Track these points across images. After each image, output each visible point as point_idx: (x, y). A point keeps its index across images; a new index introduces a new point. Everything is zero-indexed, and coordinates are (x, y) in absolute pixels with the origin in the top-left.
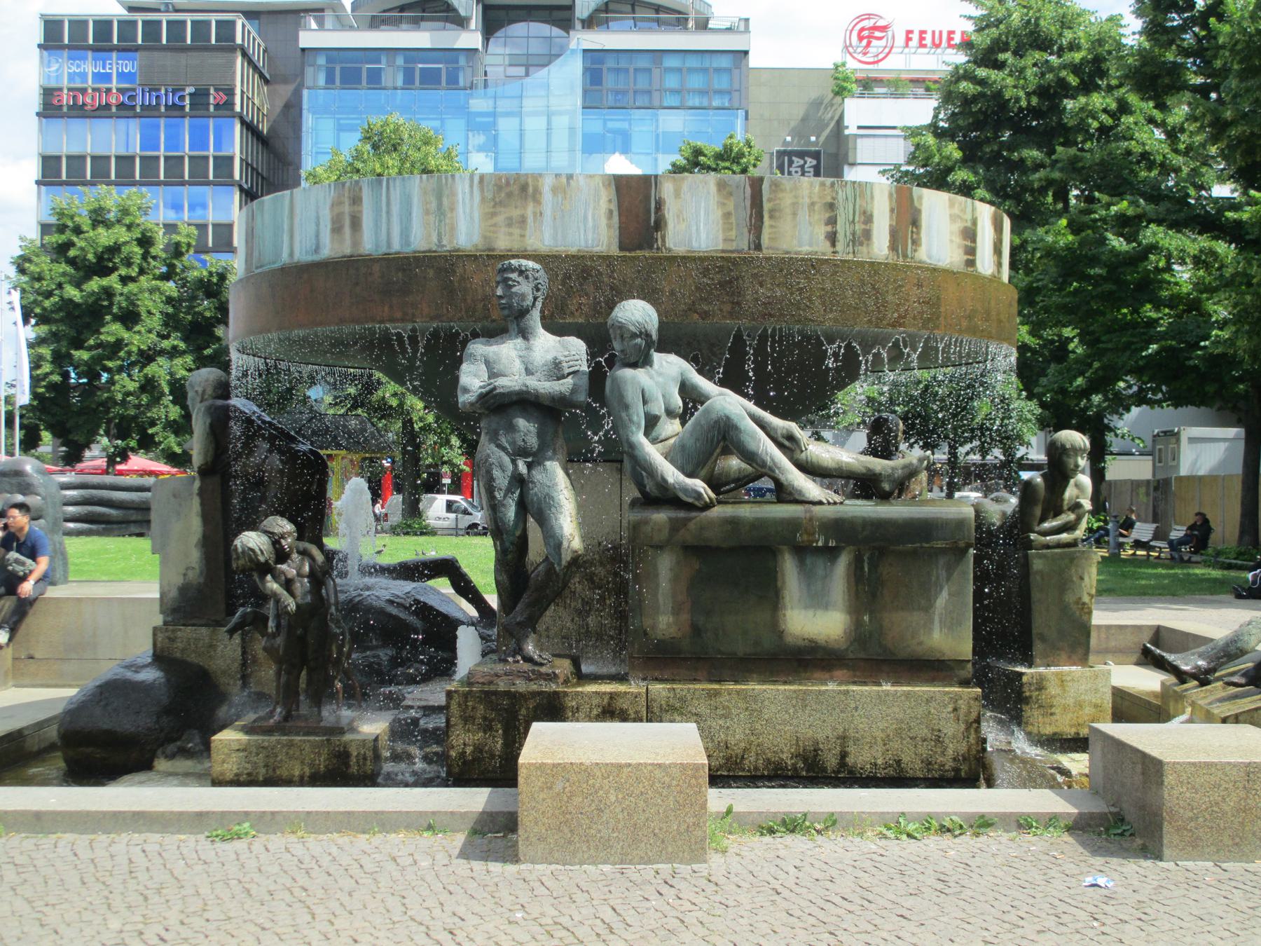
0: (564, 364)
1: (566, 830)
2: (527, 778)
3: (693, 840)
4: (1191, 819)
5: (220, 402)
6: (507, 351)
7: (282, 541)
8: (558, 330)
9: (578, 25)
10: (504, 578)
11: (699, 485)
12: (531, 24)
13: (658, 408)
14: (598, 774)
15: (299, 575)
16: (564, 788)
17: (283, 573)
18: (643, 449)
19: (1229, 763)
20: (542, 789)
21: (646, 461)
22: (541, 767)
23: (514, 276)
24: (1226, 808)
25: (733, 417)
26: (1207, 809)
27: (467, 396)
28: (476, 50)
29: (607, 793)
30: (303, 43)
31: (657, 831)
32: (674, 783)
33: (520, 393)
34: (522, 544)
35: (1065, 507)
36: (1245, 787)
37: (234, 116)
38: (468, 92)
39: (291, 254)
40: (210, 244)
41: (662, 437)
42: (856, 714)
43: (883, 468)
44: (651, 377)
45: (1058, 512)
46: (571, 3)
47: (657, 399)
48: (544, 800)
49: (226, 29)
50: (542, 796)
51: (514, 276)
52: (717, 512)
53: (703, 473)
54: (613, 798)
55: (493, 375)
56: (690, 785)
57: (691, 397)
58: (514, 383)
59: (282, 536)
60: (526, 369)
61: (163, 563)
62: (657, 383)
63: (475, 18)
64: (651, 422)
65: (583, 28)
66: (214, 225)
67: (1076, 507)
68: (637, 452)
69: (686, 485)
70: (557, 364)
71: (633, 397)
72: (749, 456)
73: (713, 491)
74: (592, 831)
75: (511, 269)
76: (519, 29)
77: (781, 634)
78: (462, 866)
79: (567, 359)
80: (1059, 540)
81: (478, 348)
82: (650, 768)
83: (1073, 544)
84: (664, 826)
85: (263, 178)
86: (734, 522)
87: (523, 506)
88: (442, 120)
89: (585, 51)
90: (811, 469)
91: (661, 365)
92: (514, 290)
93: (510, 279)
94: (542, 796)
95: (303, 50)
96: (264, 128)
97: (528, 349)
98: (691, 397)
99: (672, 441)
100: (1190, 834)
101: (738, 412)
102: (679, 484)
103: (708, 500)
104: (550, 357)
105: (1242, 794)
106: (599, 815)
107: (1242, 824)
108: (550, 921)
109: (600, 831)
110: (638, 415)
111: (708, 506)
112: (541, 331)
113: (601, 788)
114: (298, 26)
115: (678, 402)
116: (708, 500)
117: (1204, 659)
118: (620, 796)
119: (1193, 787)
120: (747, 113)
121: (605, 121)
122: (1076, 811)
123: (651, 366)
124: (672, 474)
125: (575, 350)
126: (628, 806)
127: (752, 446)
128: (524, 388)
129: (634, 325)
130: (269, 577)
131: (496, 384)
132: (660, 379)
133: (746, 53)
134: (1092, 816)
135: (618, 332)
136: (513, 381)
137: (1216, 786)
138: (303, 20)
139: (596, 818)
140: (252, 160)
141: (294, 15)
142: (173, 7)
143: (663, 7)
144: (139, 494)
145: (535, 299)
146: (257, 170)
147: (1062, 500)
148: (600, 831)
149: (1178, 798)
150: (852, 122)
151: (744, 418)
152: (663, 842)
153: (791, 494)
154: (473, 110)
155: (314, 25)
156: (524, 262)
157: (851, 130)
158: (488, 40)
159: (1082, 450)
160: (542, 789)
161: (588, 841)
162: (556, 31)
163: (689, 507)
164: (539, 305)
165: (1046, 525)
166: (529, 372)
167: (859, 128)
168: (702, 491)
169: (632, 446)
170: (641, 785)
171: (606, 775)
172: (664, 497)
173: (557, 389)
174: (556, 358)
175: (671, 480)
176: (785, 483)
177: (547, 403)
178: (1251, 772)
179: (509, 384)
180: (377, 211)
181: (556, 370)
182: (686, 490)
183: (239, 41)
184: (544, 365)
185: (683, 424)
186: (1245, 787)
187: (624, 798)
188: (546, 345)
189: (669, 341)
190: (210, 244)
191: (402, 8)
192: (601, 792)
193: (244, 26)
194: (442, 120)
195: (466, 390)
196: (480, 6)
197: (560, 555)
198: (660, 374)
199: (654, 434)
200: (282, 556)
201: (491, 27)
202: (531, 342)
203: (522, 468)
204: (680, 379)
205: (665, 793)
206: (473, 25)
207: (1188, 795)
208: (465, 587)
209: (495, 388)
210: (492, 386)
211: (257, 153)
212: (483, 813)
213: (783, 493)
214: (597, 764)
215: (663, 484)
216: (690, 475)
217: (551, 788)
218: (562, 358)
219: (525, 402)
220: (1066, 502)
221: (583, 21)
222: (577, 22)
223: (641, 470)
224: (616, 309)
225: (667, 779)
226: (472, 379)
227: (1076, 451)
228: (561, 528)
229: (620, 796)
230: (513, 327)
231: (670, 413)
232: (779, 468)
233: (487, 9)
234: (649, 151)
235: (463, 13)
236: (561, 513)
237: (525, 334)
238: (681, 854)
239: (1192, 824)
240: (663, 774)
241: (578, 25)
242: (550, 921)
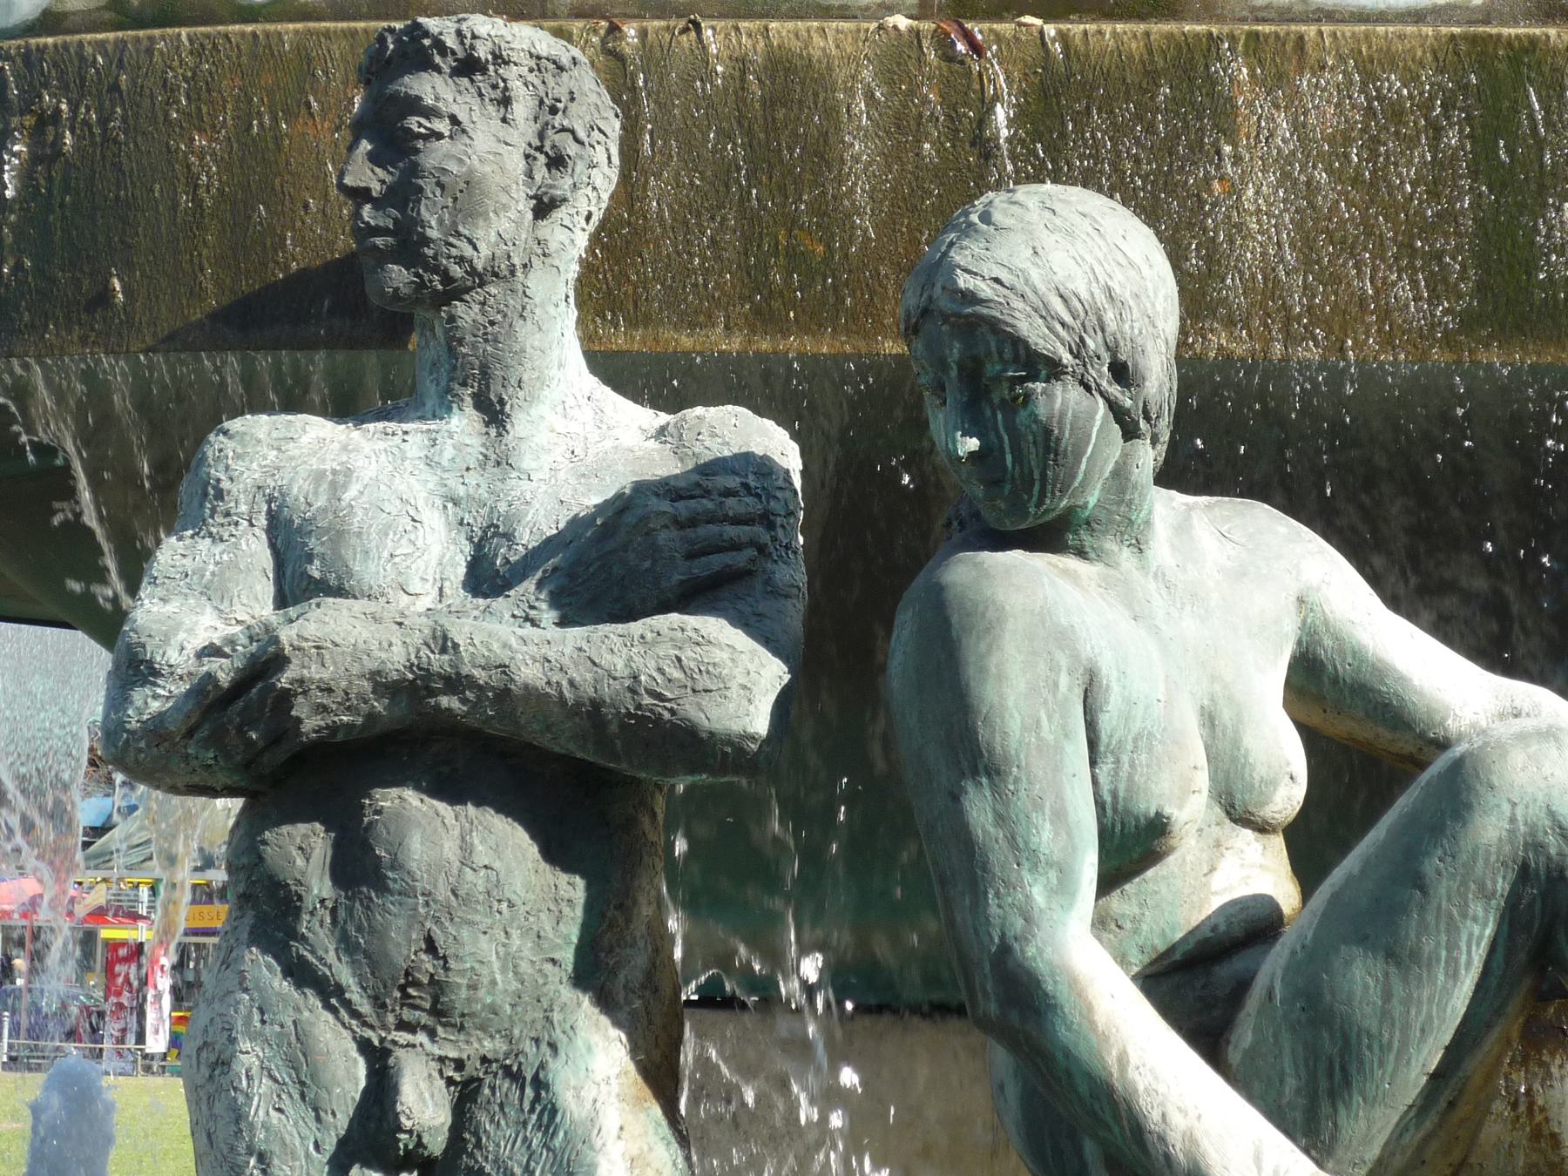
25: (1081, 977)
129: (1047, 315)
177: (564, 743)
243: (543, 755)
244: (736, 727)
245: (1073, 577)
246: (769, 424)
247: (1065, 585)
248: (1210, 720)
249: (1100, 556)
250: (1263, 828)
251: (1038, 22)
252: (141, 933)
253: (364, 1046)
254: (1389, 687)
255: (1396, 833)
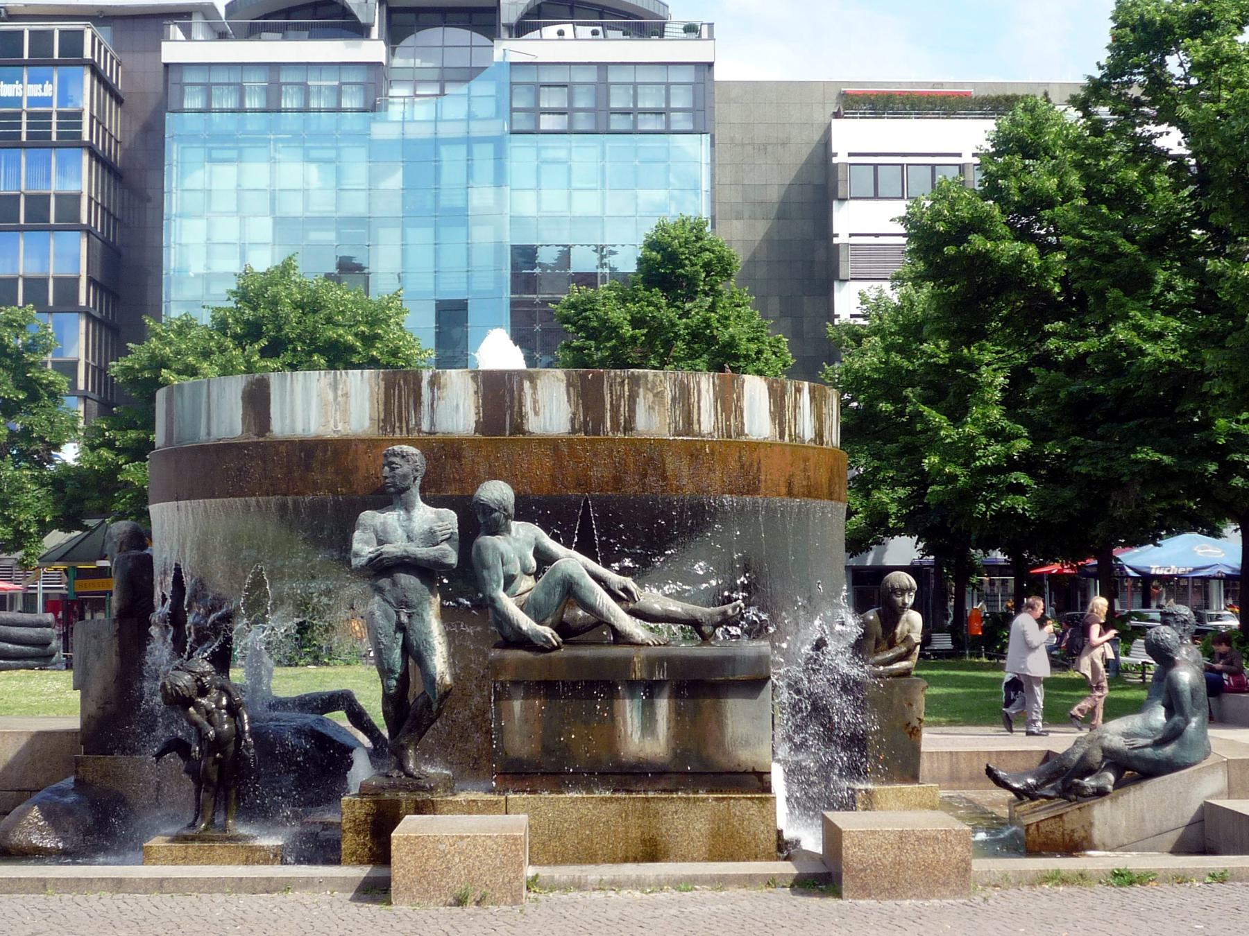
0: (439, 533)
1: (425, 883)
4: (861, 870)
5: (135, 552)
6: (391, 519)
9: (504, 34)
11: (547, 631)
12: (446, 29)
13: (516, 569)
15: (219, 708)
20: (407, 854)
23: (397, 460)
24: (886, 862)
25: (575, 576)
27: (358, 559)
28: (381, 63)
29: (454, 855)
30: (166, 58)
32: (500, 849)
33: (401, 558)
34: (404, 680)
37: (83, 145)
38: (371, 114)
39: (209, 434)
40: (51, 302)
45: (892, 644)
46: (495, 5)
49: (72, 42)
50: (408, 859)
51: (397, 460)
52: (564, 652)
53: (549, 620)
55: (381, 542)
57: (544, 559)
59: (203, 674)
60: (408, 536)
61: (84, 698)
63: (374, 17)
64: (509, 580)
65: (510, 36)
66: (56, 280)
67: (907, 639)
68: (498, 605)
70: (432, 533)
71: (490, 558)
72: (589, 608)
75: (395, 454)
76: (433, 35)
77: (617, 754)
78: (353, 908)
80: (890, 670)
81: (367, 516)
83: (906, 673)
85: (115, 218)
87: (407, 649)
88: (338, 149)
89: (512, 64)
90: (639, 614)
91: (518, 532)
92: (397, 471)
93: (394, 463)
94: (408, 859)
95: (167, 65)
96: (117, 156)
97: (410, 519)
98: (544, 559)
99: (526, 595)
102: (532, 630)
104: (426, 527)
105: (898, 852)
107: (897, 873)
109: (448, 883)
110: (498, 575)
111: (554, 648)
113: (449, 853)
114: (162, 36)
115: (533, 563)
117: (1033, 777)
119: (863, 848)
120: (713, 137)
121: (539, 149)
124: (526, 623)
125: (449, 519)
127: (591, 600)
128: (405, 554)
133: (711, 65)
134: (810, 876)
136: (397, 547)
137: (879, 847)
138: (166, 29)
140: (109, 203)
141: (156, 20)
142: (6, 11)
143: (609, 9)
145: (415, 479)
146: (109, 213)
147: (895, 634)
148: (448, 883)
150: (841, 148)
151: (584, 577)
154: (374, 137)
155: (179, 35)
156: (405, 448)
157: (840, 158)
158: (394, 50)
159: (910, 590)
160: (407, 854)
162: (479, 39)
163: (542, 650)
164: (418, 482)
165: (879, 658)
166: (410, 539)
167: (850, 155)
168: (550, 636)
169: (493, 600)
173: (432, 553)
174: (431, 529)
175: (524, 628)
179: (394, 550)
181: (431, 538)
182: (538, 635)
183: (87, 54)
184: (421, 534)
185: (537, 578)
188: (424, 515)
189: (524, 511)
191: (288, 13)
193: (93, 37)
194: (338, 149)
195: (357, 555)
196: (384, 7)
197: (434, 688)
198: (516, 540)
199: (511, 589)
200: (203, 692)
201: (394, 36)
203: (404, 619)
206: (375, 32)
208: (358, 717)
209: (381, 554)
211: (109, 189)
215: (518, 630)
216: (540, 623)
218: (436, 528)
219: (407, 564)
220: (898, 636)
221: (509, 27)
222: (502, 28)
225: (495, 846)
226: (363, 547)
227: (904, 591)
228: (435, 668)
231: (526, 572)
233: (391, 12)
234: (593, 185)
235: (362, 19)
237: (408, 508)
241: (504, 34)
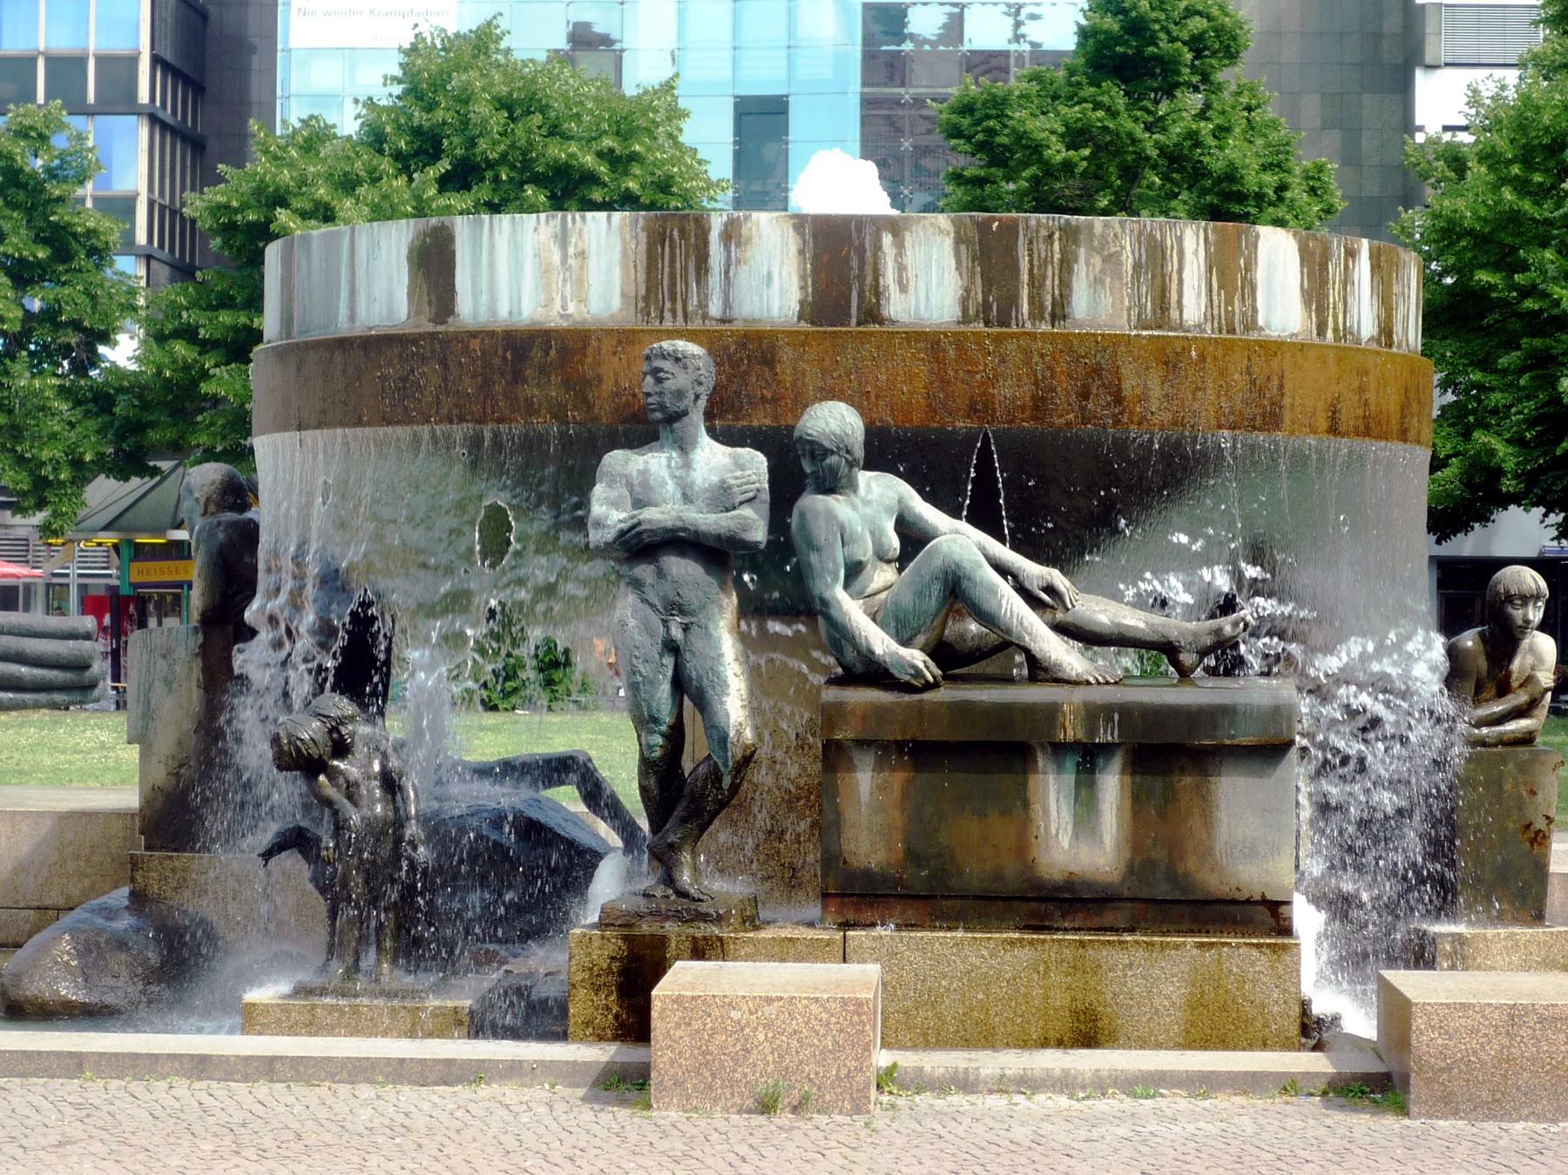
0: (736, 489)
2: (663, 1010)
3: (855, 1088)
6: (655, 463)
7: (342, 728)
8: (728, 438)
10: (652, 782)
14: (745, 1008)
16: (705, 1025)
17: (341, 772)
18: (841, 607)
19: (1490, 1005)
20: (678, 1025)
21: (840, 620)
22: (678, 1000)
25: (965, 564)
26: (1463, 1058)
31: (812, 1076)
32: (833, 1020)
33: (674, 530)
34: (676, 736)
35: (1515, 684)
36: (1508, 1033)
40: (91, 97)
41: (869, 591)
42: (1130, 973)
43: (1181, 633)
44: (855, 508)
45: (1504, 689)
47: (862, 538)
48: (681, 1037)
51: (667, 365)
52: (946, 694)
53: (921, 639)
54: (761, 1037)
56: (851, 1022)
57: (913, 538)
58: (666, 516)
61: (145, 756)
62: (863, 517)
64: (854, 570)
69: (902, 657)
71: (821, 532)
73: (939, 666)
74: (737, 1075)
75: (663, 356)
79: (739, 482)
80: (1500, 733)
81: (617, 460)
82: (805, 1002)
83: (1527, 739)
84: (821, 1069)
86: (964, 710)
87: (680, 684)
97: (687, 465)
100: (1442, 1088)
101: (973, 558)
103: (931, 679)
104: (715, 479)
105: (1505, 1041)
106: (744, 1056)
107: (1505, 1077)
108: (679, 1154)
112: (705, 440)
113: (748, 1024)
115: (894, 542)
116: (931, 679)
118: (770, 1035)
119: (1447, 1033)
122: (1331, 1070)
123: (855, 491)
124: (881, 643)
126: (779, 1046)
127: (989, 605)
129: (831, 440)
130: (322, 778)
131: (641, 517)
132: (868, 510)
135: (808, 447)
136: (663, 514)
137: (1474, 1031)
139: (741, 1060)
144: (71, 643)
145: (697, 397)
148: (745, 1075)
149: (1428, 1046)
151: (980, 566)
152: (819, 1088)
153: (1046, 670)
160: (678, 1025)
161: (732, 1087)
163: (907, 688)
164: (702, 403)
166: (687, 498)
168: (921, 665)
170: (794, 1022)
171: (753, 1010)
172: (874, 673)
174: (723, 482)
175: (879, 650)
176: (1038, 656)
177: (711, 543)
178: (1553, 1019)
180: (476, 263)
181: (723, 497)
182: (901, 661)
184: (706, 490)
185: (900, 570)
186: (1508, 1033)
187: (773, 1037)
190: (91, 97)
192: (748, 1030)
195: (599, 524)
198: (867, 503)
202: (691, 456)
204: (896, 508)
205: (822, 1032)
207: (1440, 1041)
208: (595, 794)
209: (639, 523)
210: (635, 521)
212: (608, 1063)
213: (1039, 670)
214: (744, 997)
215: (868, 657)
216: (906, 643)
217: (689, 1024)
218: (732, 482)
220: (1514, 676)
223: (840, 637)
224: (806, 417)
225: (825, 1016)
228: (727, 715)
229: (770, 1035)
230: (664, 433)
231: (882, 557)
232: (1030, 634)
236: (728, 695)
237: (684, 446)
238: (840, 1103)
239: (1445, 1076)
240: (821, 1009)
242: (679, 1154)
243: (705, 546)
244: (753, 539)
245: (837, 500)
246: (758, 453)
247: (835, 503)
248: (872, 534)
249: (845, 494)
250: (888, 562)
251: (783, 657)
252: (181, 535)
253: (663, 620)
254: (922, 524)
255: (915, 567)
